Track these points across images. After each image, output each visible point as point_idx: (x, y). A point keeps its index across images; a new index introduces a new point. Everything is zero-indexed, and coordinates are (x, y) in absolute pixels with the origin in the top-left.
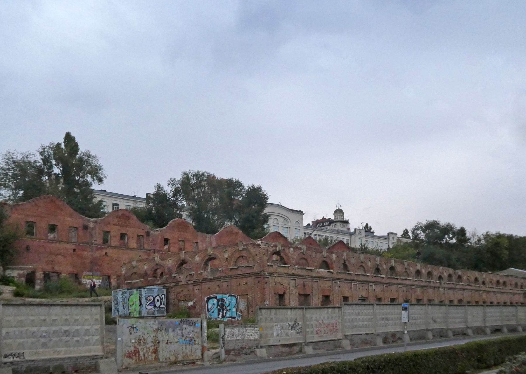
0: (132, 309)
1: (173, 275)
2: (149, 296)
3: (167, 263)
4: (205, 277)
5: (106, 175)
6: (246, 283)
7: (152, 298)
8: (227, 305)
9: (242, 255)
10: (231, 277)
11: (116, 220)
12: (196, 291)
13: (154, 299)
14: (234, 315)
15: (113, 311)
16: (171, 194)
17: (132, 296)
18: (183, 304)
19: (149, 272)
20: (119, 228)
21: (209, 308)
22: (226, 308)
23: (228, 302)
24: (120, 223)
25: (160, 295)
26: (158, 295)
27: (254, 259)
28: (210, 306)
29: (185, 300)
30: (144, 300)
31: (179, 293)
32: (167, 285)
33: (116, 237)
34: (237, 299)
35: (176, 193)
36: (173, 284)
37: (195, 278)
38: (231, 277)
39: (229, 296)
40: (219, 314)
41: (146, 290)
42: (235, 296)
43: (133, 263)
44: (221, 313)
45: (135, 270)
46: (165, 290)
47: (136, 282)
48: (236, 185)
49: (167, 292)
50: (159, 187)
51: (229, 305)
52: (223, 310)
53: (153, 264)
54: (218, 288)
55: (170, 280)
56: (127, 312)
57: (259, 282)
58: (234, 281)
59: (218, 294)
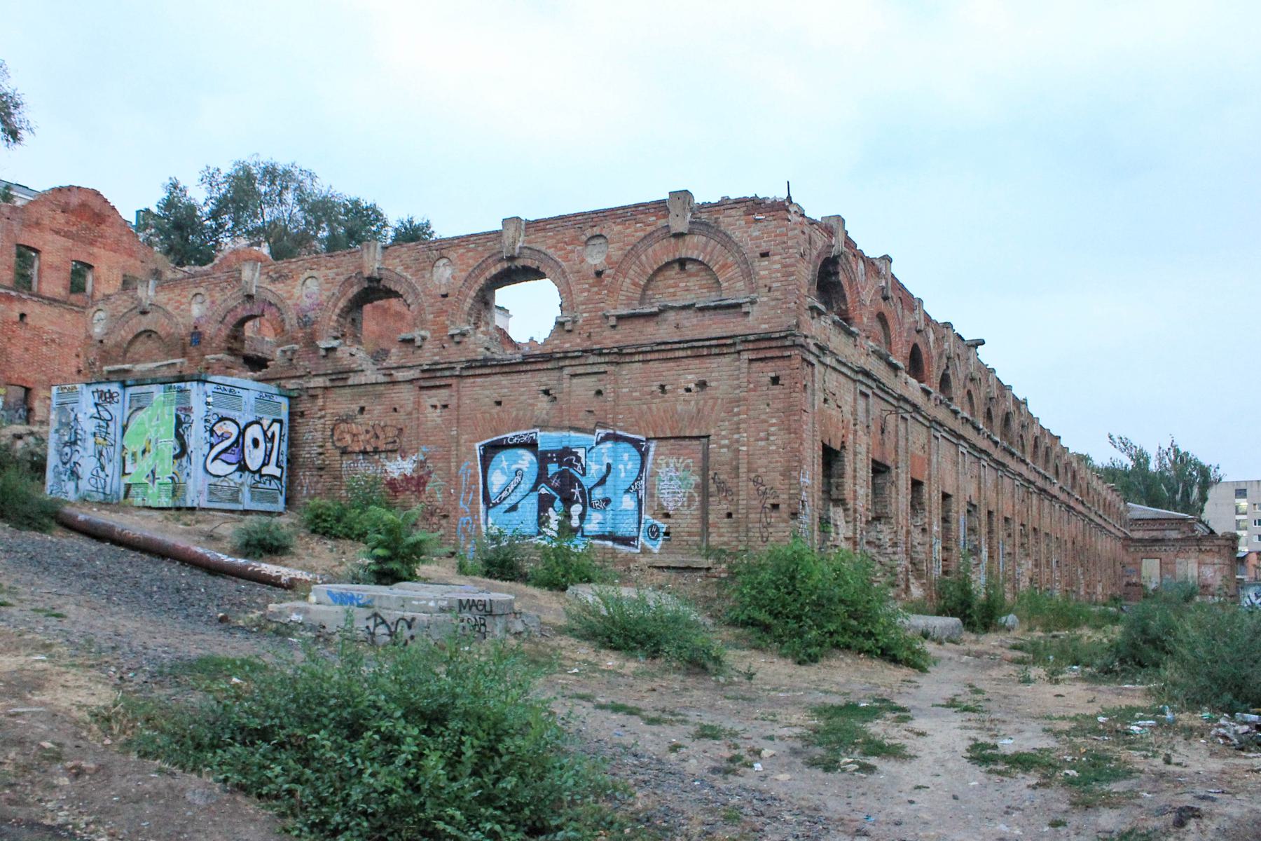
0: (137, 471)
1: (323, 344)
2: (222, 419)
3: (297, 292)
4: (481, 353)
5: (32, 125)
6: (702, 385)
7: (234, 430)
9: (684, 254)
10: (620, 355)
11: (61, 218)
12: (434, 416)
13: (242, 433)
14: (627, 527)
15: (50, 474)
16: (207, 209)
17: (141, 414)
18: (364, 469)
19: (209, 330)
20: (69, 243)
21: (494, 489)
23: (595, 471)
24: (74, 229)
25: (266, 423)
26: (258, 422)
27: (748, 274)
28: (497, 480)
29: (376, 451)
30: (197, 437)
31: (347, 419)
32: (291, 384)
33: (57, 269)
34: (643, 455)
35: (221, 206)
36: (319, 382)
37: (428, 356)
38: (620, 355)
39: (604, 440)
40: (542, 521)
41: (209, 388)
42: (635, 443)
43: (141, 292)
44: (554, 516)
45: (145, 323)
46: (284, 402)
48: (368, 216)
49: (292, 414)
51: (602, 482)
52: (568, 501)
53: (228, 298)
54: (543, 403)
55: (304, 364)
56: (116, 484)
57: (775, 381)
58: (631, 372)
59: (544, 427)
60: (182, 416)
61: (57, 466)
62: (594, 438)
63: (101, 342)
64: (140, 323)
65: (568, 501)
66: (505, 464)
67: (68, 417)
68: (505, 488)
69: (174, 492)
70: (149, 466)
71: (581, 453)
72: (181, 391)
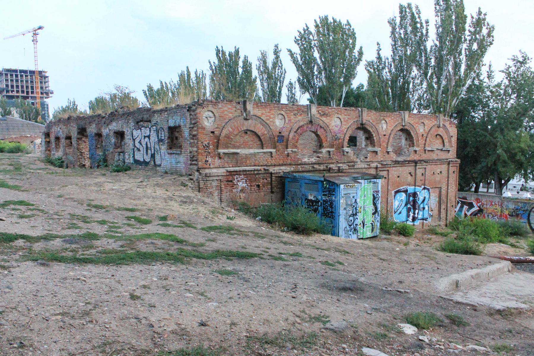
6: (441, 172)
14: (426, 216)
22: (419, 207)
28: (396, 204)
40: (408, 216)
44: (411, 214)
47: (255, 154)
52: (415, 209)
61: (346, 227)
62: (421, 188)
63: (213, 132)
64: (243, 125)
66: (398, 198)
67: (351, 201)
68: (398, 206)
69: (372, 230)
71: (418, 193)
72: (374, 183)
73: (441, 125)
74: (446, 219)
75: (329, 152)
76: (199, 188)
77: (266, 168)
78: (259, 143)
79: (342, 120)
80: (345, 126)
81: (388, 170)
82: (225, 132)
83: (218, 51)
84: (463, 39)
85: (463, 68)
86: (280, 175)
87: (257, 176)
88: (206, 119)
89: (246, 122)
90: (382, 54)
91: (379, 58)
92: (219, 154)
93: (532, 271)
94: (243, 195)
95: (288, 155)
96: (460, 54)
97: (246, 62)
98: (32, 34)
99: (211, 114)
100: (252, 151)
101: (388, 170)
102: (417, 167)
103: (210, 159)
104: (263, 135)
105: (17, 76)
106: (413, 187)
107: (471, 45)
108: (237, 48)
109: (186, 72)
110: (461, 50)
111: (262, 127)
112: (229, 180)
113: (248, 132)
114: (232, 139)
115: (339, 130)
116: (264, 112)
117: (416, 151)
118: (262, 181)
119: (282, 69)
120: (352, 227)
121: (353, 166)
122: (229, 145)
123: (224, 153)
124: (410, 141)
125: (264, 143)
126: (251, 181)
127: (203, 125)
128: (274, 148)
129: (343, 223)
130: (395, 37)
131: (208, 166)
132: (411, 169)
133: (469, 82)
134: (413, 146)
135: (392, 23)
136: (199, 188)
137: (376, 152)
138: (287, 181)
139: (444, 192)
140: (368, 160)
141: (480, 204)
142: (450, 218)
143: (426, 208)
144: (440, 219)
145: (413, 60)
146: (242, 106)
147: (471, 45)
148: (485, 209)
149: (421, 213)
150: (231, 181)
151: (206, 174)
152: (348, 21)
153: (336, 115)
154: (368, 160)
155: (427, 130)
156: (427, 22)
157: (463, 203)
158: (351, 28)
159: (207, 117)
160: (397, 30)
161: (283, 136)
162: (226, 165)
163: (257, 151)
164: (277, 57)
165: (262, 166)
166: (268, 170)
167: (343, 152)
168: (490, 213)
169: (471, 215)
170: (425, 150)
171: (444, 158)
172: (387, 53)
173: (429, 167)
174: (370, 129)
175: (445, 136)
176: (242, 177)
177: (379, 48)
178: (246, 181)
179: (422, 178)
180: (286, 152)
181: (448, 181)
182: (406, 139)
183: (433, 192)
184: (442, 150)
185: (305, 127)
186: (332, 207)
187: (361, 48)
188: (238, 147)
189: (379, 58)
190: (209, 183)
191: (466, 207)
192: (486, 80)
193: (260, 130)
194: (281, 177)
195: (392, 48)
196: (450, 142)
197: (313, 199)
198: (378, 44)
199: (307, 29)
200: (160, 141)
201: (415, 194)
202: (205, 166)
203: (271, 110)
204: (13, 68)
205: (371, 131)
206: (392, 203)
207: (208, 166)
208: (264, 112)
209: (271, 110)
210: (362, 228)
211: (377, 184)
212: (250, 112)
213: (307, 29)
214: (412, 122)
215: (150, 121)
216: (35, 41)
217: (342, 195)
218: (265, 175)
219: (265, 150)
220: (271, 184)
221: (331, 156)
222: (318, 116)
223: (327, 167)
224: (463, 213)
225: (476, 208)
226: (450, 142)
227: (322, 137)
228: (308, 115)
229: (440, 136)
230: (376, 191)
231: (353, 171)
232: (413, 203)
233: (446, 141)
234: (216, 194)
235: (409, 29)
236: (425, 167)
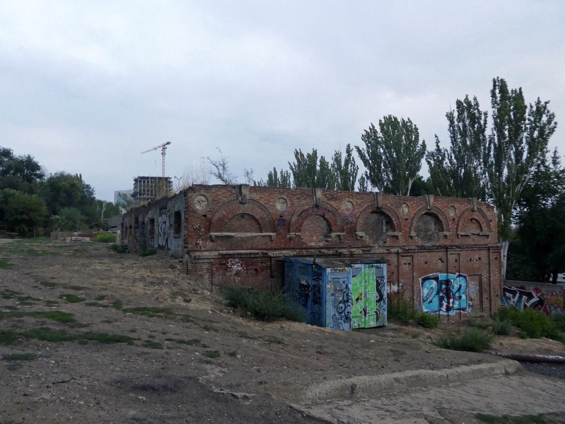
6: (480, 258)
8: (454, 290)
14: (464, 305)
22: (454, 295)
28: (425, 292)
40: (441, 305)
44: (445, 304)
47: (253, 238)
50: (77, 175)
52: (449, 298)
60: (379, 281)
61: (335, 315)
62: (455, 276)
63: (205, 216)
65: (449, 298)
66: (428, 285)
67: (341, 286)
69: (377, 319)
70: (361, 307)
71: (452, 281)
73: (476, 209)
74: (491, 310)
75: (339, 236)
76: (188, 270)
77: (265, 251)
78: (257, 226)
79: (354, 204)
80: (358, 210)
81: (412, 256)
82: (218, 215)
83: (297, 154)
84: (523, 128)
85: (525, 155)
86: (280, 259)
87: (254, 260)
88: (198, 203)
89: (242, 206)
90: (441, 146)
91: (438, 150)
92: (211, 237)
93: (563, 377)
94: (238, 279)
95: (291, 239)
96: (521, 142)
97: (323, 161)
98: (161, 148)
99: (203, 198)
100: (249, 234)
101: (412, 256)
102: (449, 253)
103: (200, 242)
104: (262, 218)
105: (148, 182)
106: (445, 274)
107: (531, 134)
108: (315, 149)
109: (273, 173)
110: (522, 138)
111: (260, 210)
112: (222, 262)
113: (246, 216)
114: (226, 222)
115: (350, 214)
116: (263, 196)
117: (446, 236)
118: (260, 265)
119: (354, 166)
120: (343, 314)
121: (370, 251)
122: (223, 228)
123: (216, 236)
124: (440, 225)
125: (262, 226)
126: (247, 265)
127: (195, 209)
128: (274, 232)
129: (330, 310)
130: (454, 130)
131: (199, 248)
132: (441, 254)
133: (533, 169)
134: (443, 231)
135: (450, 117)
136: (188, 270)
137: (396, 237)
138: (286, 264)
139: (485, 279)
140: (387, 244)
141: (540, 294)
142: (495, 310)
143: (464, 297)
144: (482, 309)
145: (474, 150)
146: (238, 190)
147: (531, 134)
148: (546, 301)
149: (457, 302)
150: (224, 264)
151: (195, 257)
152: (409, 119)
153: (347, 199)
154: (387, 244)
155: (459, 214)
156: (486, 114)
157: (522, 294)
158: (413, 125)
159: (199, 201)
160: (456, 123)
161: (285, 220)
162: (219, 248)
163: (254, 234)
164: (349, 155)
165: (260, 249)
166: (266, 253)
167: (356, 236)
168: (552, 304)
169: (531, 306)
170: (458, 235)
171: (482, 243)
172: (446, 144)
173: (463, 253)
174: (388, 213)
175: (482, 220)
176: (237, 260)
177: (437, 140)
178: (242, 265)
179: (456, 264)
180: (288, 236)
181: (489, 268)
182: (435, 224)
183: (471, 280)
184: (478, 235)
185: (310, 211)
186: (319, 293)
187: (424, 142)
188: (234, 231)
189: (438, 150)
190: (198, 265)
191: (524, 297)
192: (551, 166)
193: (258, 213)
194: (282, 261)
195: (452, 140)
196: (489, 226)
197: (305, 284)
198: (436, 136)
199: (373, 129)
200: (171, 225)
201: (447, 282)
202: (196, 249)
203: (270, 194)
204: (146, 176)
205: (390, 215)
206: (420, 291)
207: (199, 248)
208: (263, 196)
209: (270, 194)
210: (363, 316)
211: (381, 269)
212: (245, 196)
213: (373, 129)
214: (439, 206)
215: (166, 208)
216: (163, 154)
217: (329, 280)
218: (264, 259)
219: (263, 234)
220: (271, 269)
221: (342, 240)
222: (325, 200)
223: (337, 251)
224: (522, 304)
225: (535, 299)
226: (489, 226)
227: (330, 220)
228: (313, 198)
229: (475, 219)
230: (381, 277)
231: (369, 256)
232: (446, 291)
233: (484, 226)
234: (207, 276)
235: (467, 122)
236: (458, 252)
